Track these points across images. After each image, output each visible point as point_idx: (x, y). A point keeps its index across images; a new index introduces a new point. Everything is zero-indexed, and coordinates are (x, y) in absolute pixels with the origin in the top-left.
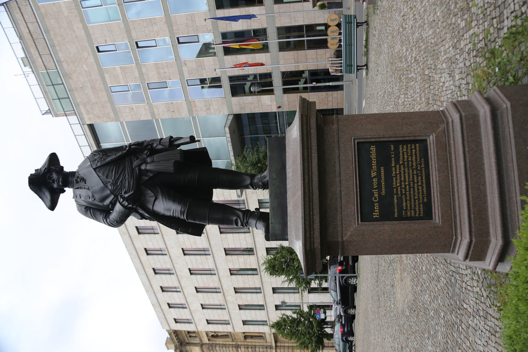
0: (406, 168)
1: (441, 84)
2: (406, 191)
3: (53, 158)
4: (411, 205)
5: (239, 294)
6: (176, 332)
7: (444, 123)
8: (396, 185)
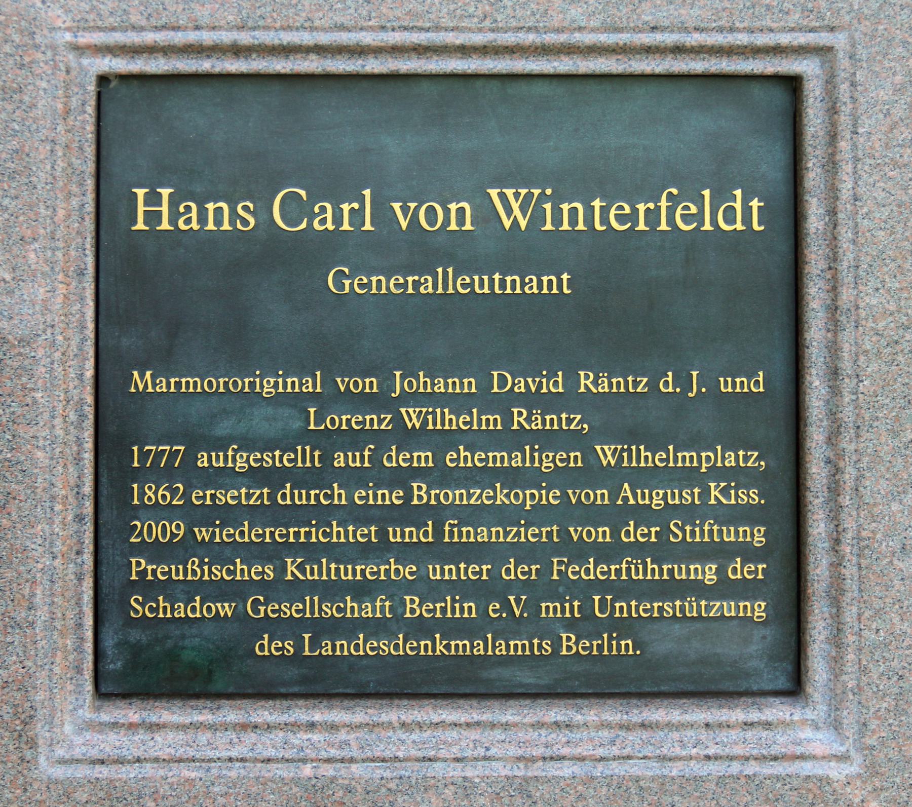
0: (553, 497)
2: (354, 478)
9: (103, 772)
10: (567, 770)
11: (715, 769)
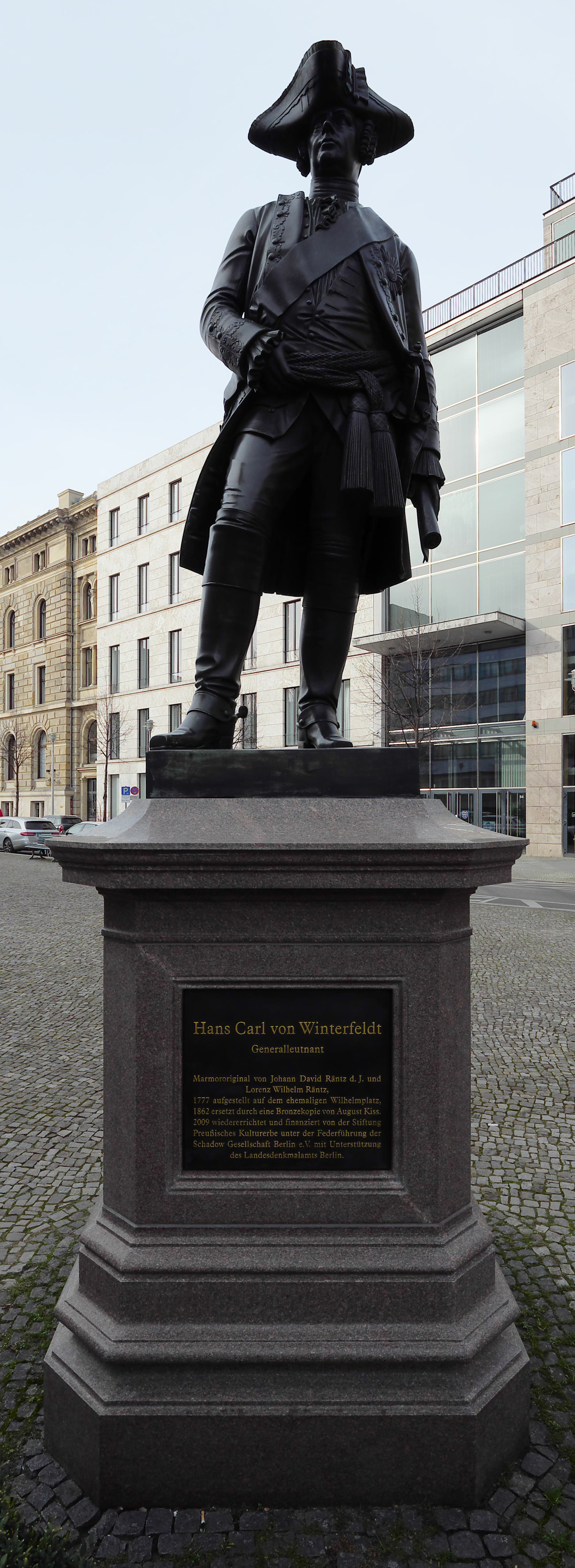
0: (318, 1112)
1: (555, 1133)
2: (259, 1107)
3: (393, 130)
4: (223, 1118)
5: (167, 640)
6: (92, 511)
7: (434, 1222)
8: (275, 1084)
9: (185, 1193)
10: (321, 1193)
11: (365, 1193)
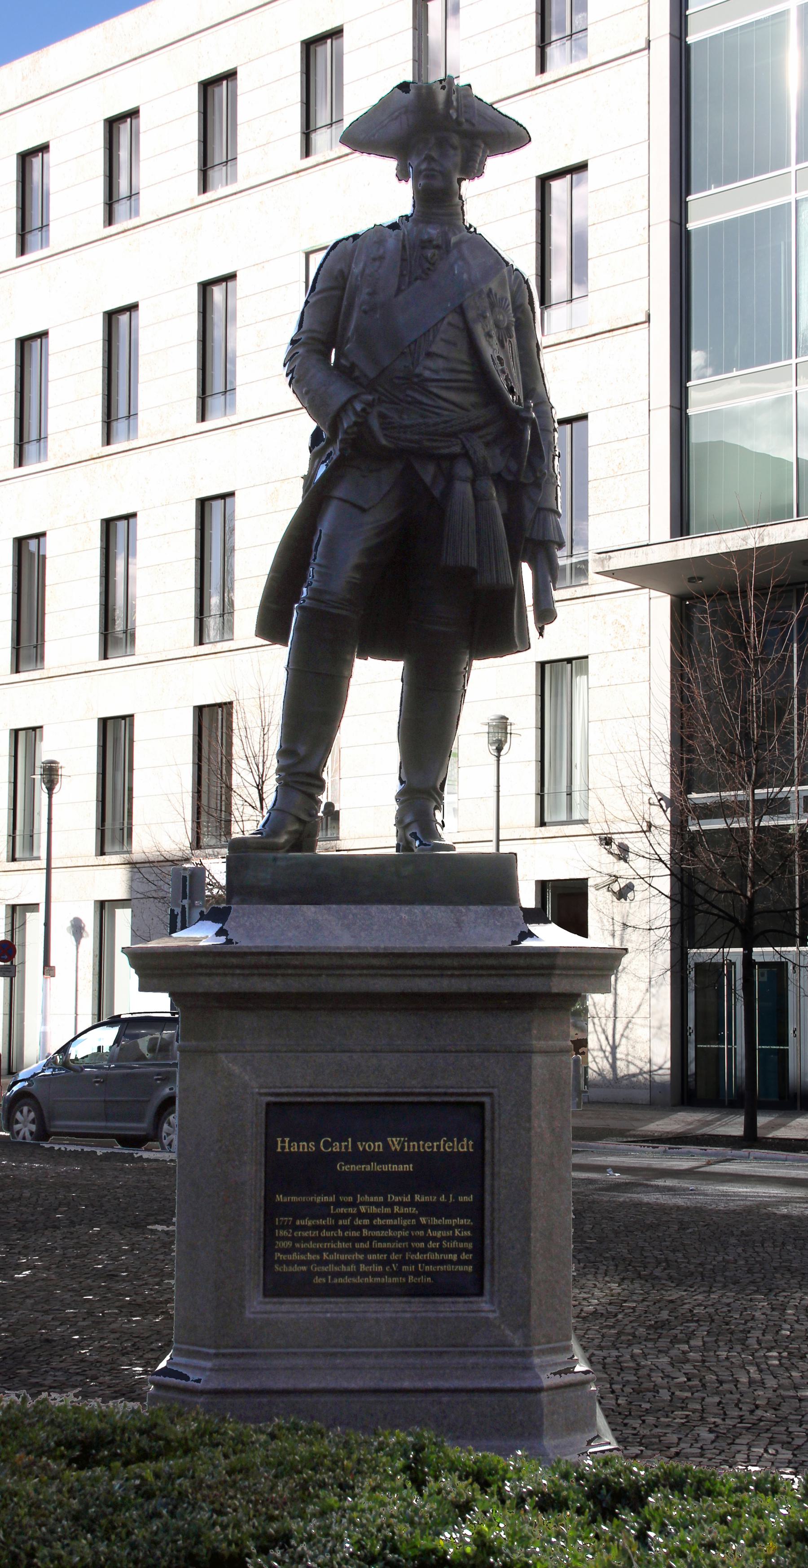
2: (344, 1228)
4: (307, 1240)
8: (362, 1203)
9: (265, 1316)
